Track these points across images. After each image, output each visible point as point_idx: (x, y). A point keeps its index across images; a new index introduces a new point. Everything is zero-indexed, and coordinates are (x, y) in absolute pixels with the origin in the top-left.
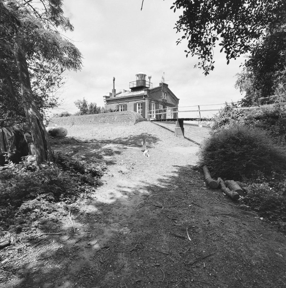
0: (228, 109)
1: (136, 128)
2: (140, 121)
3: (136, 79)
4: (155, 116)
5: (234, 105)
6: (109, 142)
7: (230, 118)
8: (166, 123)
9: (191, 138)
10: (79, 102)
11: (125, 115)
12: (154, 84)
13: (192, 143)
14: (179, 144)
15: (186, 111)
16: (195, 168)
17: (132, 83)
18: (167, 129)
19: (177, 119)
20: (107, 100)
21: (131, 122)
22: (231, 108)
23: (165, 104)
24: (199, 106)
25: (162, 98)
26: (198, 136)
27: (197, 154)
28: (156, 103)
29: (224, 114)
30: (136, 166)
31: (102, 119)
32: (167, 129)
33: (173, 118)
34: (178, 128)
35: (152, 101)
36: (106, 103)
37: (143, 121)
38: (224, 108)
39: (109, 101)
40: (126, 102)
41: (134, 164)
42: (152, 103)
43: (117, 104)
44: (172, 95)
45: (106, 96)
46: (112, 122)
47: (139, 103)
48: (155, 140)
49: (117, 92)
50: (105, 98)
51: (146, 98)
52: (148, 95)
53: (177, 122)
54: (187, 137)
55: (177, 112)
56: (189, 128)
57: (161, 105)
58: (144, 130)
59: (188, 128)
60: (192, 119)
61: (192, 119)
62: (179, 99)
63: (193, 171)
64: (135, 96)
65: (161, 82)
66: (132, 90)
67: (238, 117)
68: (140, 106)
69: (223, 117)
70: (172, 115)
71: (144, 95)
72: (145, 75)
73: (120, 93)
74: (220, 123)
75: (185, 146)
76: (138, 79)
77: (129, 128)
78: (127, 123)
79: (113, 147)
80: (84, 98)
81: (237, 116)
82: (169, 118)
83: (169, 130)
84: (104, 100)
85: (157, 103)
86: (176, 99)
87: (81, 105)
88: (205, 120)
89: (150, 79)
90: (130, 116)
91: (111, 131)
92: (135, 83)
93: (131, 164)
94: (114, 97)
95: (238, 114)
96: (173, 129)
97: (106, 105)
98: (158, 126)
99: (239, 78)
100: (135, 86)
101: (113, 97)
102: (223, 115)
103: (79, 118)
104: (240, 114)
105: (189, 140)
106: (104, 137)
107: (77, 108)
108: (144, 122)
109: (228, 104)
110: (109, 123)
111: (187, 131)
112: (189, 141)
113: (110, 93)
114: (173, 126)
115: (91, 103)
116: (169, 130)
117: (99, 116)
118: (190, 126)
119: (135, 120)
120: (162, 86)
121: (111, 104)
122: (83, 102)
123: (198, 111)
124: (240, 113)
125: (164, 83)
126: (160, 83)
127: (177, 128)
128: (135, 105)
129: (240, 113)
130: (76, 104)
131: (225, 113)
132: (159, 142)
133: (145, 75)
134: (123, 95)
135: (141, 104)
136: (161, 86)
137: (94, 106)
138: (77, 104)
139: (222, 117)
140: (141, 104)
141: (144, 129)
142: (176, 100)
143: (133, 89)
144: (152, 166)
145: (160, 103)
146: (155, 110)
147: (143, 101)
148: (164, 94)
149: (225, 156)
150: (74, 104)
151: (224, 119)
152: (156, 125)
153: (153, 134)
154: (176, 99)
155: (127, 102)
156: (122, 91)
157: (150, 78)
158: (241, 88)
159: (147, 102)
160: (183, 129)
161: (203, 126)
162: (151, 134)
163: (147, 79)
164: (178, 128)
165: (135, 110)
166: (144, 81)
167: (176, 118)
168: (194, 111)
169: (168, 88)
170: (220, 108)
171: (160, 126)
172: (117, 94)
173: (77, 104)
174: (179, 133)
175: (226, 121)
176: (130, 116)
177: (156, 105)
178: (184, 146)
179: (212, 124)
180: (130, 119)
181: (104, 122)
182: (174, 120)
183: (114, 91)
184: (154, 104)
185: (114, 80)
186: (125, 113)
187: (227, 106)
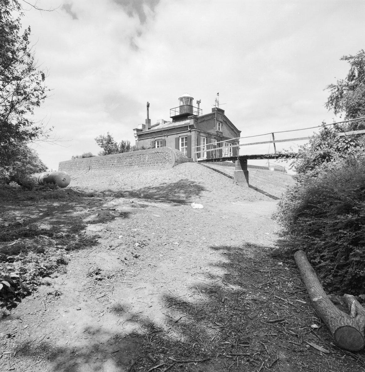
0: (326, 134)
1: (174, 173)
2: (182, 162)
3: (179, 103)
4: (205, 153)
5: (338, 128)
6: (120, 195)
7: (332, 150)
8: (221, 165)
9: (260, 187)
10: (102, 138)
11: (160, 154)
12: (206, 109)
13: (261, 194)
14: (241, 197)
15: (251, 144)
16: (276, 255)
17: (174, 110)
18: (222, 173)
19: (237, 157)
20: (138, 134)
21: (168, 164)
22: (333, 132)
23: (220, 137)
24: (273, 133)
25: (216, 129)
26: (269, 183)
27: (274, 217)
28: (206, 137)
29: (321, 144)
30: (146, 249)
31: (128, 160)
32: (222, 173)
33: (232, 155)
34: (239, 170)
35: (202, 134)
36: (138, 138)
37: (186, 162)
38: (319, 134)
39: (141, 135)
40: (165, 136)
41: (143, 245)
42: (201, 137)
43: (153, 140)
44: (230, 126)
45: (137, 129)
46: (142, 164)
47: (182, 137)
48: (199, 189)
49: (152, 123)
50: (136, 131)
51: (192, 130)
52: (195, 125)
53: (237, 162)
54: (254, 186)
55: (237, 145)
56: (255, 172)
57: (215, 140)
58: (185, 175)
59: (254, 172)
60: (261, 157)
61: (261, 157)
62: (241, 132)
63: (271, 260)
64: (177, 127)
65: (214, 107)
66: (173, 120)
67: (347, 148)
68: (184, 142)
69: (319, 149)
70: (230, 154)
71: (190, 126)
72: (191, 99)
73: (158, 125)
74: (314, 160)
75: (251, 200)
76: (182, 104)
77: (165, 172)
78: (162, 165)
79: (122, 205)
80: (108, 133)
81: (345, 147)
82: (226, 156)
83: (224, 174)
84: (135, 134)
85: (209, 136)
86: (235, 131)
87: (105, 142)
88: (26, 328)
89: (199, 104)
90: (167, 154)
91: (137, 178)
92: (178, 109)
93: (137, 244)
94: (148, 130)
95: (347, 143)
96: (232, 174)
97: (137, 141)
98: (209, 169)
99: (333, 91)
100: (178, 114)
101: (146, 130)
102: (319, 146)
103: (97, 159)
104: (352, 143)
105: (256, 189)
106: (125, 186)
107: (99, 147)
108: (188, 163)
109: (328, 127)
110: (137, 166)
111: (253, 176)
112: (256, 191)
113: (143, 125)
114: (232, 169)
115: (123, 142)
116: (224, 174)
117: (124, 157)
118: (257, 169)
119: (174, 161)
120: (216, 112)
121: (145, 140)
122: (107, 138)
123: (271, 142)
124: (351, 141)
125: (219, 108)
126: (212, 109)
127: (237, 171)
128: (177, 140)
129: (351, 141)
130: (98, 141)
131: (323, 143)
132: (203, 193)
133: (191, 99)
134: (162, 126)
135: (186, 138)
136: (214, 112)
137: (126, 145)
138: (100, 141)
139: (318, 150)
140: (186, 138)
141: (186, 173)
142: (237, 133)
143: (176, 119)
144: (181, 250)
145: (213, 137)
146: (205, 144)
147: (189, 134)
148: (219, 124)
149: (356, 234)
150: (96, 142)
151: (322, 153)
152: (206, 168)
153: (198, 181)
154: (235, 131)
155: (166, 137)
156: (161, 122)
157: (198, 102)
158: (335, 108)
159: (193, 135)
160: (246, 173)
161: (276, 170)
162: (196, 181)
163: (194, 104)
164: (239, 170)
165: (177, 147)
166: (191, 107)
167: (236, 156)
168: (264, 143)
169: (224, 115)
170: (311, 135)
171: (212, 169)
172: (154, 126)
173: (100, 141)
174: (241, 180)
175: (326, 157)
176: (167, 154)
177: (207, 139)
178: (249, 200)
179: (300, 162)
180: (167, 159)
181: (131, 165)
182: (233, 159)
183: (148, 121)
184: (204, 139)
185: (148, 106)
186: (160, 151)
187: (326, 130)
